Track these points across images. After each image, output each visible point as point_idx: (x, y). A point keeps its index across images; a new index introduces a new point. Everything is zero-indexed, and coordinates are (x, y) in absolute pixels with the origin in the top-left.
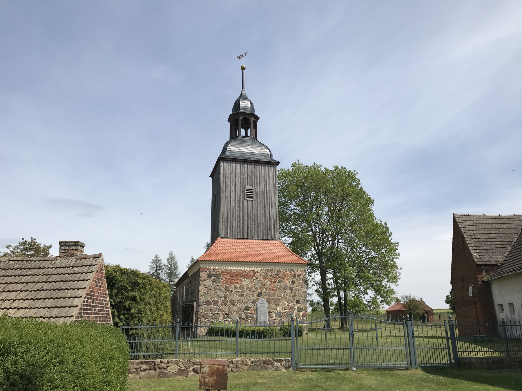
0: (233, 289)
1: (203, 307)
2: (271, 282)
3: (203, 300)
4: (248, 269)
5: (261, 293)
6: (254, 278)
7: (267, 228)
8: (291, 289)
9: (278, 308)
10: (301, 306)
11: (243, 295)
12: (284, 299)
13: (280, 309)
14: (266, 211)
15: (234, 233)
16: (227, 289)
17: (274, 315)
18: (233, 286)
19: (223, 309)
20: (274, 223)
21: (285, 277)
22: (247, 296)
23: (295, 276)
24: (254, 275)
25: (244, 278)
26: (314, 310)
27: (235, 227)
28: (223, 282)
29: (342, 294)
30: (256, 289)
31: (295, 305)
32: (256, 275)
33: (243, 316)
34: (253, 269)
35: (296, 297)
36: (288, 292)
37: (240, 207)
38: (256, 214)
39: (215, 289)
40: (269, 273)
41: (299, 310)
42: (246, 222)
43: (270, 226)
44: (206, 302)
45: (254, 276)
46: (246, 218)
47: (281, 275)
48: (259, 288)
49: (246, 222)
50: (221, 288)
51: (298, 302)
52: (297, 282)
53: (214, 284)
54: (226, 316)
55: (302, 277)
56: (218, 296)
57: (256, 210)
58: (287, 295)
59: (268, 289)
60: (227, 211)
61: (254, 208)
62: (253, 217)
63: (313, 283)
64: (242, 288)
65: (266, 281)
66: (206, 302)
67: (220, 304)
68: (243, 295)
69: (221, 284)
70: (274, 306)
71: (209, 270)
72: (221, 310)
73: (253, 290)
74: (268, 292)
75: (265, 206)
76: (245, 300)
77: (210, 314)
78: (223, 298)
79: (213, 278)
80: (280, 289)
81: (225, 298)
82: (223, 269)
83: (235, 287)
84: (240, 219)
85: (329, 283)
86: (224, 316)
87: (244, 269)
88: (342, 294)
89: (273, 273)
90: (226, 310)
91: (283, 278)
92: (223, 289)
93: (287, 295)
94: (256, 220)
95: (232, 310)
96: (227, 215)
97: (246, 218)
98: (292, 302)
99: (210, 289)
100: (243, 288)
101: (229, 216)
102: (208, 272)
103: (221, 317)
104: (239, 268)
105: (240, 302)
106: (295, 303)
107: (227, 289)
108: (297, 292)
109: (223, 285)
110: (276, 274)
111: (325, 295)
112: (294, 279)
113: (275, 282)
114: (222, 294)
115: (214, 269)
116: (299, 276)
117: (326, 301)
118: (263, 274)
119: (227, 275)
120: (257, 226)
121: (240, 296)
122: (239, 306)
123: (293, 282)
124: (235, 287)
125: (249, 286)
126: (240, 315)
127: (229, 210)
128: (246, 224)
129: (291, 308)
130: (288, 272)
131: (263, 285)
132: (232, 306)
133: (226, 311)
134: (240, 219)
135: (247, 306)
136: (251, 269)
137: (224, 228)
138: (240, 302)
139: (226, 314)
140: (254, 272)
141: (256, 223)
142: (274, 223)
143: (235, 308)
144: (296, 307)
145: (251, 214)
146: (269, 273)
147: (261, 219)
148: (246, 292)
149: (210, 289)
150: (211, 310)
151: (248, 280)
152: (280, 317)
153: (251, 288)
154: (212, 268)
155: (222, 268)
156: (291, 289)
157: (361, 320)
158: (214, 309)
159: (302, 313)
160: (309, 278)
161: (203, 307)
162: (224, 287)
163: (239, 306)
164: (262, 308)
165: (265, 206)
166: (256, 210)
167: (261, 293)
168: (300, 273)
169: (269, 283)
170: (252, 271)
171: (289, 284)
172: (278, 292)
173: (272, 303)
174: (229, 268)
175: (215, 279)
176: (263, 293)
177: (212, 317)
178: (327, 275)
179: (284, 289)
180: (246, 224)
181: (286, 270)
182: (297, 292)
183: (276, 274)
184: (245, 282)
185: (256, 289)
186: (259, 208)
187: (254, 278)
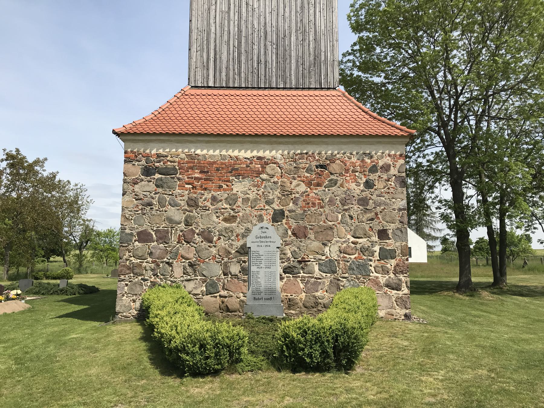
0: (208, 204)
1: (130, 247)
2: (309, 184)
3: (132, 229)
4: (249, 154)
5: (282, 213)
6: (264, 176)
7: (309, 59)
8: (363, 202)
9: (327, 249)
10: (391, 244)
11: (234, 217)
12: (342, 229)
13: (332, 251)
14: (306, 21)
15: (224, 74)
16: (193, 203)
17: (316, 268)
18: (208, 195)
19: (182, 251)
20: (326, 47)
21: (347, 171)
22: (246, 219)
23: (373, 169)
24: (263, 167)
25: (237, 176)
26: (444, 250)
27: (228, 61)
28: (181, 187)
29: (496, 223)
30: (269, 203)
31: (373, 244)
32: (268, 169)
33: (235, 269)
34: (261, 154)
35: (376, 222)
36: (356, 209)
37: (240, 13)
38: (281, 29)
39: (161, 203)
40: (303, 163)
41: (386, 254)
42: (255, 47)
43: (317, 57)
44: (139, 234)
45: (263, 172)
46: (256, 39)
47: (335, 167)
48: (277, 201)
49: (255, 47)
50: (178, 200)
51: (383, 234)
52: (379, 185)
53: (160, 190)
54: (189, 270)
55: (393, 171)
56: (170, 220)
57: (280, 19)
58: (351, 217)
59: (300, 203)
60: (209, 24)
61: (274, 14)
62: (272, 37)
63: (437, 204)
64: (232, 200)
65: (295, 182)
66: (139, 234)
67: (174, 239)
68: (234, 217)
69: (178, 191)
70: (315, 245)
71: (147, 157)
72: (176, 255)
73: (262, 204)
74: (299, 211)
75: (302, 7)
76: (241, 230)
77: (148, 263)
78: (182, 226)
79: (157, 176)
80: (331, 202)
81: (187, 224)
82: (183, 156)
83: (214, 199)
84: (240, 43)
85: (468, 206)
86: (185, 268)
87: (236, 153)
88: (496, 223)
89: (314, 163)
90: (191, 255)
91: (341, 174)
92: (182, 203)
93: (351, 217)
94: (281, 43)
95: (204, 254)
96: (208, 34)
97: (256, 39)
98: (366, 235)
99: (150, 204)
100: (236, 201)
101: (213, 36)
102: (143, 162)
103: (178, 271)
104: (224, 152)
105: (225, 234)
106: (375, 238)
107: (193, 203)
108: (379, 209)
109: (182, 194)
110: (322, 166)
111: (462, 222)
112: (372, 177)
113: (319, 185)
114: (177, 215)
115: (159, 156)
116: (386, 168)
117: (463, 236)
118: (286, 167)
119: (192, 168)
120: (283, 57)
121: (226, 220)
122: (222, 243)
123: (369, 185)
124: (214, 199)
125: (251, 196)
126: (226, 265)
127: (212, 21)
128: (256, 52)
129: (363, 250)
130: (354, 159)
131: (286, 193)
132: (205, 244)
133: (191, 255)
134: (240, 43)
135: (244, 246)
136: (255, 153)
137: (199, 64)
138: (225, 234)
139: (191, 265)
140: (264, 162)
141: (281, 49)
142: (326, 47)
143: (214, 251)
144: (377, 248)
145: (269, 29)
146: (303, 163)
147: (293, 38)
148: (244, 210)
149: (150, 204)
150: (151, 254)
151: (247, 183)
152: (334, 272)
153: (255, 200)
154: (154, 152)
155: (178, 152)
156: (363, 202)
157: (524, 268)
158: (157, 253)
159: (393, 262)
160: (428, 195)
161: (130, 247)
162: (186, 198)
163: (222, 243)
164: (262, 250)
165: (302, 7)
166: (280, 19)
167: (282, 213)
168: (388, 160)
169: (303, 188)
170: (259, 158)
171: (356, 189)
172: (327, 209)
173: (312, 236)
174: (198, 152)
175: (161, 179)
176: (287, 213)
177: (152, 270)
178: (465, 190)
179: (344, 202)
180: (256, 52)
181: (350, 155)
182: (379, 209)
183: (322, 166)
184: (239, 187)
185: (269, 203)
186: (287, 14)
187: (264, 176)
